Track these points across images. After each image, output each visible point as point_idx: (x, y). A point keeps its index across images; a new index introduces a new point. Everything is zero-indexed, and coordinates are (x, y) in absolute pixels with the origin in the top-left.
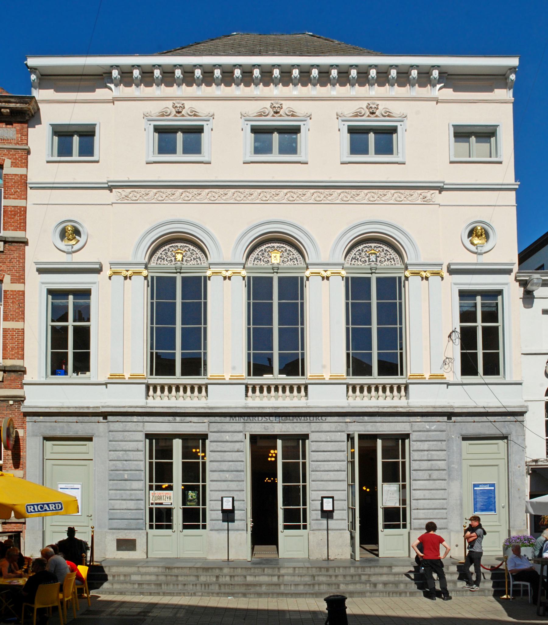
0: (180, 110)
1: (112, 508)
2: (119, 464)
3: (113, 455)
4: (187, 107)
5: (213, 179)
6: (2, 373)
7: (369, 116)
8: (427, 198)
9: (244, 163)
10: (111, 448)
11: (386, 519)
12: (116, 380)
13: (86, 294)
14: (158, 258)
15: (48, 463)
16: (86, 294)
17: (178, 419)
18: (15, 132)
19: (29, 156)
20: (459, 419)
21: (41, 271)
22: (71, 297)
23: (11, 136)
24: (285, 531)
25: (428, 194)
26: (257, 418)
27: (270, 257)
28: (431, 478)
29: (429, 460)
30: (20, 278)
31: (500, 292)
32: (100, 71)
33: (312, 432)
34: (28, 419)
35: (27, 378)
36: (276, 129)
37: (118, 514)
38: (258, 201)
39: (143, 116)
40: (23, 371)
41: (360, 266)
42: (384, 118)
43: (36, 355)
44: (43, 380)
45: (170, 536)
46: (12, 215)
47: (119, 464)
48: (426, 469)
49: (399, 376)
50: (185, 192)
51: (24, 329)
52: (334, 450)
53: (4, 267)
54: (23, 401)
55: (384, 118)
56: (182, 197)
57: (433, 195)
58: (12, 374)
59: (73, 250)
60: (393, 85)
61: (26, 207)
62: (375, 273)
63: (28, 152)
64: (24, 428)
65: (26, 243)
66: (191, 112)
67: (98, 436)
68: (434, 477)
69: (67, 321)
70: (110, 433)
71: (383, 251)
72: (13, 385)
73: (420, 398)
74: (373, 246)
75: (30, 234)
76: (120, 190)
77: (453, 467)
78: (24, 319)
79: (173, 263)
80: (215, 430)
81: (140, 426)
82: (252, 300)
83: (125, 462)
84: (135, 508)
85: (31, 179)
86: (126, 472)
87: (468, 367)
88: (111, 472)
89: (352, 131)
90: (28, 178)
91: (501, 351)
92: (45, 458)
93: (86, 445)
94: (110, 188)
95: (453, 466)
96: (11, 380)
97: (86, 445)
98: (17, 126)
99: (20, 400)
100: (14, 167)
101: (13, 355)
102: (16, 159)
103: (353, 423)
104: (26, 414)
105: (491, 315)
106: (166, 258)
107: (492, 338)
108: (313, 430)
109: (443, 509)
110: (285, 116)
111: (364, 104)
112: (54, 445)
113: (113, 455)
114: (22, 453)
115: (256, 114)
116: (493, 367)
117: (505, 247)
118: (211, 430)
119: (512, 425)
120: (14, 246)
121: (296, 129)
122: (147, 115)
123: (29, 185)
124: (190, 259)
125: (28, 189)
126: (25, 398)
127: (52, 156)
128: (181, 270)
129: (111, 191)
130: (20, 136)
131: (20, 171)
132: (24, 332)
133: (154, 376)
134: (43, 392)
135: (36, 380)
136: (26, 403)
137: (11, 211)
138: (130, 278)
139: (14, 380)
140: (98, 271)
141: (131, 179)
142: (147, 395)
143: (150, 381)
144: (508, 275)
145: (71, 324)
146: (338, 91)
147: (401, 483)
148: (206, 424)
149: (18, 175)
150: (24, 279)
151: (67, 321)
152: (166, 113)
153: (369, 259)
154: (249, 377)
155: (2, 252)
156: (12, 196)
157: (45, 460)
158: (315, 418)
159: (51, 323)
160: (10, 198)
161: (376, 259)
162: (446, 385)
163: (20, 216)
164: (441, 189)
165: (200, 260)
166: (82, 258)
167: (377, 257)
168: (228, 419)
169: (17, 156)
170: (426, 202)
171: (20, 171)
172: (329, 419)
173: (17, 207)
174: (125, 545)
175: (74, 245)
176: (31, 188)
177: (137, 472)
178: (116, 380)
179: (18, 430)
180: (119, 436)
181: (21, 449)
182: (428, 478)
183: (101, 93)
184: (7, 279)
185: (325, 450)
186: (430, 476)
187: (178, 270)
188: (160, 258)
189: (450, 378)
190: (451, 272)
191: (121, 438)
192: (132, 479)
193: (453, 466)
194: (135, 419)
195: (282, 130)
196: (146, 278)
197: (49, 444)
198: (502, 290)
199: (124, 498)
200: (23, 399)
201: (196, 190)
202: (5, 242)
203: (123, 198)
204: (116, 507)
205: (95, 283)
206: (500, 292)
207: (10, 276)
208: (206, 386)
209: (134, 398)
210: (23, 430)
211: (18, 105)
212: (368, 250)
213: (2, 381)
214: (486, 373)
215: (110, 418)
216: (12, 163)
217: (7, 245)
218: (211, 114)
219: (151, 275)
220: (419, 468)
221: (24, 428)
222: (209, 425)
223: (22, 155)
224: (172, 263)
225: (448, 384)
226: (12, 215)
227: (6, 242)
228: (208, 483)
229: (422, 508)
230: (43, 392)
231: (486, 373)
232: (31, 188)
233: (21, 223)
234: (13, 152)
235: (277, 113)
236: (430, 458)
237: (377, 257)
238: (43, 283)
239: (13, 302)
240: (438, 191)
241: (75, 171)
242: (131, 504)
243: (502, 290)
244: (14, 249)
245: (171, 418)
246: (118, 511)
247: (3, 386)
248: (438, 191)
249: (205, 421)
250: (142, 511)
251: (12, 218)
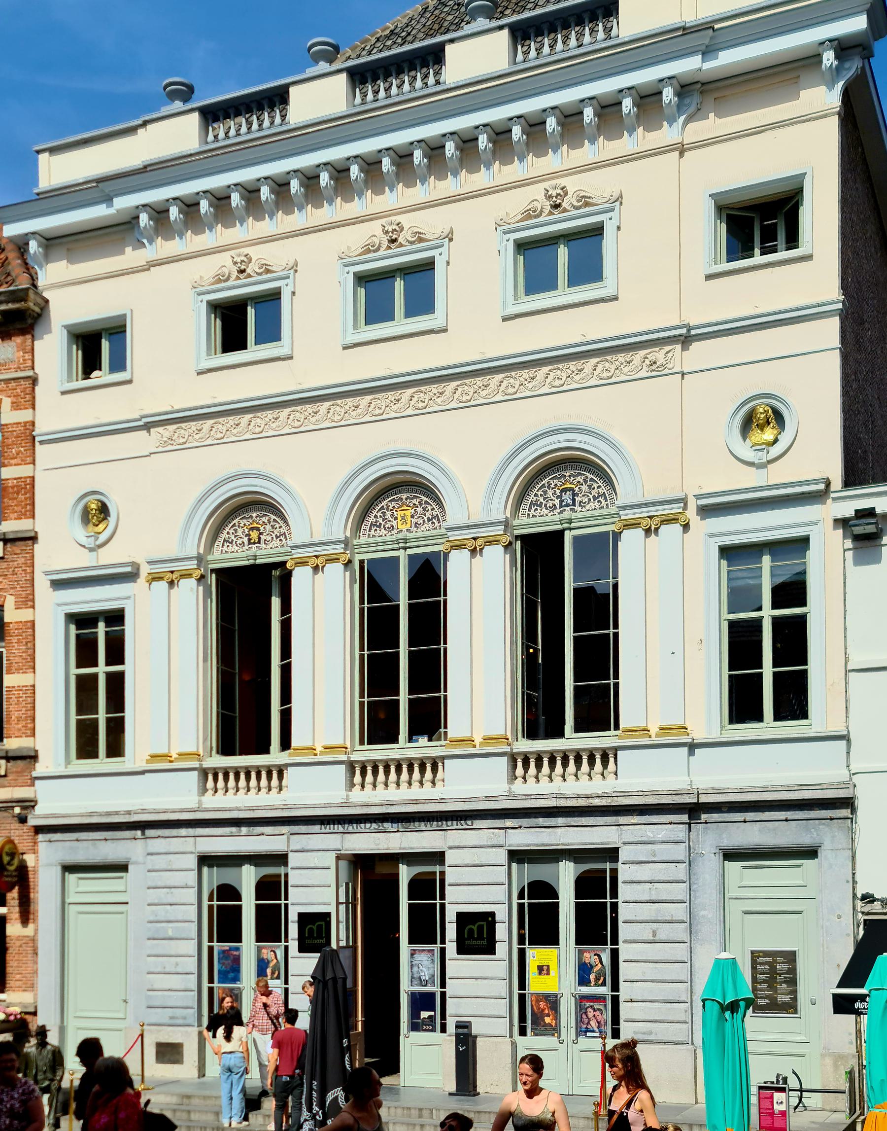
0: (394, 237)
1: (150, 988)
2: (162, 912)
3: (154, 895)
4: (571, 190)
5: (578, 340)
6: (3, 762)
7: (551, 213)
8: (658, 363)
9: (344, 348)
10: (150, 884)
11: (414, 1013)
12: (162, 764)
13: (116, 618)
14: (225, 540)
15: (72, 910)
16: (116, 618)
17: (244, 830)
18: (15, 349)
19: (36, 388)
20: (715, 817)
21: (58, 584)
22: (766, 560)
23: (10, 356)
24: (412, 1033)
25: (658, 354)
26: (362, 825)
27: (396, 519)
28: (657, 939)
29: (654, 902)
30: (28, 601)
31: (804, 541)
32: (126, 218)
33: (450, 848)
34: (41, 837)
35: (40, 769)
36: (398, 269)
37: (159, 998)
38: (499, 397)
39: (495, 226)
40: (32, 758)
41: (384, 539)
42: (259, 278)
43: (51, 726)
44: (715, 735)
45: (556, 1050)
46: (14, 493)
47: (162, 912)
48: (648, 918)
49: (612, 732)
50: (507, 377)
51: (34, 686)
52: (486, 881)
53: (5, 584)
54: (33, 807)
55: (259, 278)
56: (596, 373)
57: (670, 355)
58: (19, 762)
59: (98, 543)
60: (331, 201)
61: (33, 478)
62: (570, 529)
63: (34, 381)
64: (35, 852)
65: (34, 539)
66: (578, 201)
67: (136, 863)
68: (661, 936)
69: (96, 665)
70: (149, 857)
71: (269, 522)
72: (21, 780)
73: (640, 775)
74: (404, 497)
75: (41, 524)
76: (160, 429)
77: (703, 916)
78: (34, 668)
79: (246, 547)
80: (298, 847)
81: (498, 836)
82: (366, 605)
83: (169, 907)
84: (182, 987)
85: (40, 429)
86: (171, 925)
87: (743, 705)
88: (150, 925)
89: (362, 279)
90: (36, 425)
91: (726, 673)
92: (68, 901)
93: (122, 878)
94: (147, 427)
95: (703, 913)
96: (17, 772)
97: (799, 866)
98: (18, 340)
99: (29, 804)
100: (15, 410)
101: (19, 730)
102: (17, 396)
103: (519, 830)
104: (39, 830)
105: (792, 592)
106: (235, 540)
107: (793, 639)
108: (451, 844)
109: (679, 1002)
110: (407, 244)
111: (537, 192)
112: (745, 867)
113: (154, 895)
114: (32, 895)
115: (520, 217)
116: (793, 701)
117: (817, 443)
118: (291, 848)
119: (823, 827)
120: (17, 548)
121: (427, 264)
122: (501, 223)
123: (37, 439)
124: (586, 500)
125: (37, 444)
126: (36, 802)
127: (70, 379)
128: (256, 559)
129: (149, 432)
130: (21, 353)
131: (24, 416)
132: (34, 690)
133: (366, 747)
134: (66, 790)
135: (52, 771)
136: (38, 810)
137: (13, 487)
138: (657, 530)
139: (20, 773)
140: (131, 576)
141: (176, 407)
142: (513, 777)
143: (354, 757)
144: (132, 584)
145: (768, 614)
146: (194, 241)
147: (439, 945)
148: (285, 837)
149: (20, 423)
150: (33, 600)
151: (96, 665)
152: (373, 246)
153: (561, 502)
154: (362, 747)
155: (2, 558)
156: (13, 462)
157: (66, 906)
158: (455, 822)
159: (75, 671)
160: (11, 465)
161: (574, 500)
162: (685, 750)
163: (26, 493)
164: (686, 340)
165: (286, 537)
166: (113, 556)
167: (574, 495)
168: (316, 828)
169: (19, 391)
170: (657, 371)
171: (24, 416)
172: (478, 823)
173: (21, 478)
174: (169, 1052)
175: (100, 533)
176: (41, 442)
177: (187, 924)
178: (162, 764)
179: (25, 857)
180: (160, 862)
181: (32, 887)
182: (651, 938)
183: (131, 257)
184: (10, 604)
185: (471, 882)
186: (654, 934)
187: (402, 545)
188: (227, 541)
189: (698, 734)
190: (706, 511)
191: (164, 866)
192: (178, 936)
193: (703, 913)
194: (183, 832)
195: (405, 271)
196: (348, 564)
197: (734, 867)
198: (122, 611)
199: (167, 970)
200: (32, 804)
201: (194, 423)
202: (6, 541)
203: (165, 442)
204: (156, 987)
205: (128, 598)
206: (804, 541)
207: (13, 597)
208: (616, 750)
209: (179, 795)
210: (33, 856)
211: (11, 306)
212: (247, 524)
213: (5, 776)
214: (779, 716)
215: (149, 833)
216: (13, 403)
217: (9, 545)
218: (291, 264)
219: (359, 557)
220: (634, 918)
221: (35, 852)
222: (288, 838)
223: (27, 388)
224: (556, 512)
225: (692, 747)
226: (14, 493)
227: (6, 541)
228: (621, 946)
229: (640, 998)
230: (66, 790)
231: (779, 716)
232: (41, 442)
233: (26, 505)
234: (13, 384)
235: (393, 241)
236: (654, 898)
237: (574, 495)
238: (711, 536)
239: (19, 642)
240: (679, 347)
241: (104, 402)
242: (175, 982)
243: (122, 611)
244: (19, 551)
245: (234, 830)
246: (160, 993)
247: (6, 783)
248: (679, 347)
249: (283, 832)
250: (192, 993)
251: (15, 499)
